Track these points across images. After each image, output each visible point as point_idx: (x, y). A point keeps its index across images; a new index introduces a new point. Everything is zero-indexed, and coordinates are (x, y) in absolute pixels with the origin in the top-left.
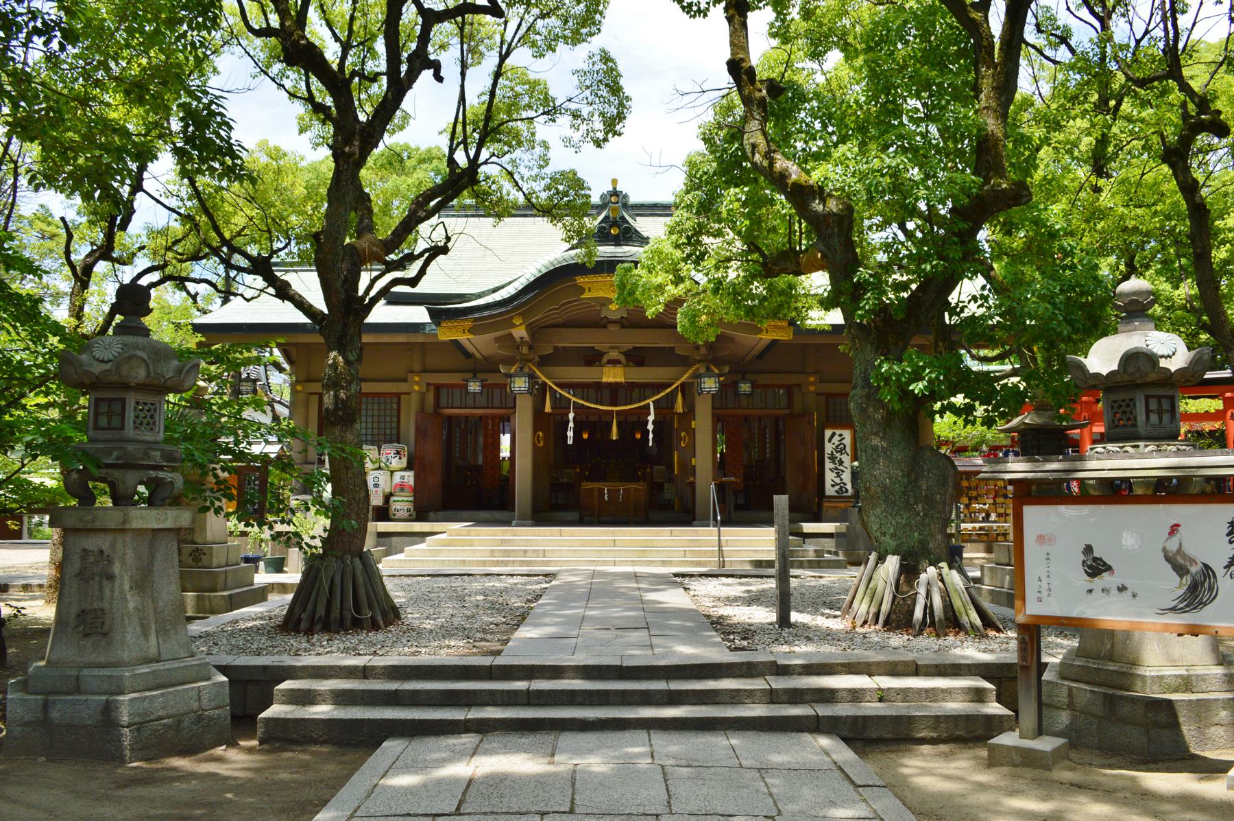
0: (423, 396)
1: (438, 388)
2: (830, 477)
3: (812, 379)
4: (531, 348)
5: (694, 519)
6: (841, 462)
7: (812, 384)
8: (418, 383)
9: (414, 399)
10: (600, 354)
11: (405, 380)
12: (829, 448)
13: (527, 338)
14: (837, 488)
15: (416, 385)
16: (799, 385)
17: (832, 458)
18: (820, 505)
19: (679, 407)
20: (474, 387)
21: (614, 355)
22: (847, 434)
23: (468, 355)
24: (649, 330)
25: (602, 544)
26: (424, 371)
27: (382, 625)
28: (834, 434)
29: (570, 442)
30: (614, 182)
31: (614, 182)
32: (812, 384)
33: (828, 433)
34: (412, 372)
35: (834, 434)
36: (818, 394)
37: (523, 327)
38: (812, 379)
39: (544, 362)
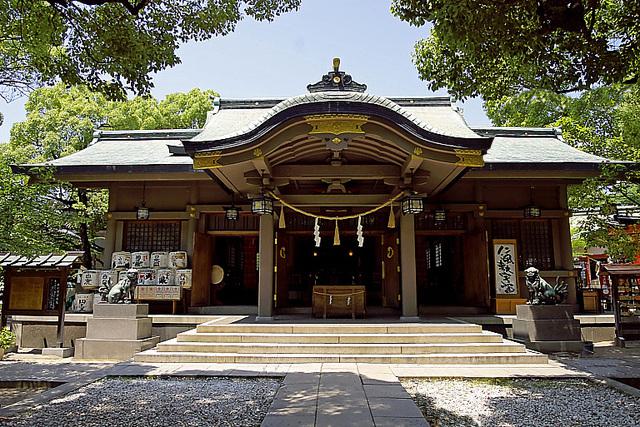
0: (197, 221)
1: (208, 216)
2: (499, 281)
3: (481, 208)
4: (271, 180)
5: (402, 315)
6: (508, 269)
7: (481, 211)
8: (193, 212)
9: (191, 225)
10: (325, 186)
11: (184, 210)
12: (498, 258)
13: (267, 172)
14: (505, 288)
15: (192, 213)
16: (472, 212)
17: (501, 266)
18: (493, 302)
19: (392, 224)
20: (232, 214)
21: (336, 185)
22: (512, 248)
23: (230, 192)
24: (364, 166)
25: (328, 340)
26: (198, 204)
27: (419, 232)
28: (502, 248)
29: (361, 245)
30: (337, 61)
31: (337, 61)
32: (481, 211)
33: (497, 248)
34: (189, 204)
35: (502, 248)
36: (486, 219)
37: (262, 158)
38: (481, 208)
39: (285, 191)
